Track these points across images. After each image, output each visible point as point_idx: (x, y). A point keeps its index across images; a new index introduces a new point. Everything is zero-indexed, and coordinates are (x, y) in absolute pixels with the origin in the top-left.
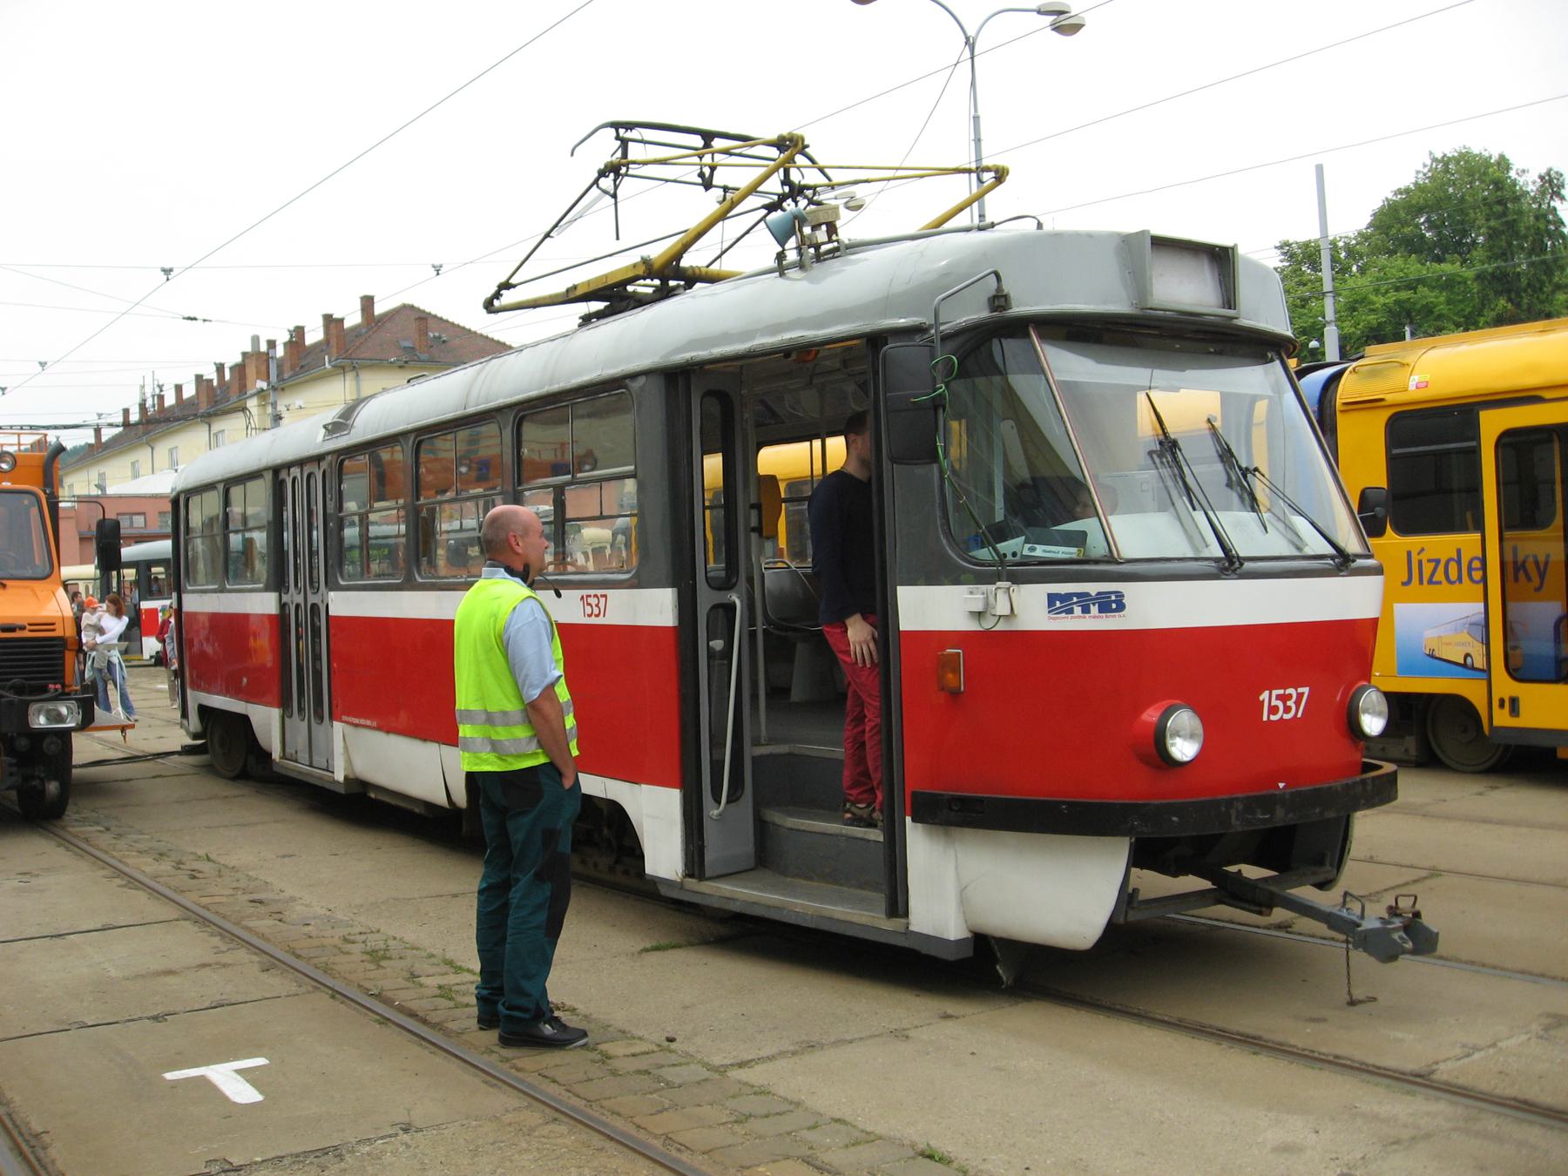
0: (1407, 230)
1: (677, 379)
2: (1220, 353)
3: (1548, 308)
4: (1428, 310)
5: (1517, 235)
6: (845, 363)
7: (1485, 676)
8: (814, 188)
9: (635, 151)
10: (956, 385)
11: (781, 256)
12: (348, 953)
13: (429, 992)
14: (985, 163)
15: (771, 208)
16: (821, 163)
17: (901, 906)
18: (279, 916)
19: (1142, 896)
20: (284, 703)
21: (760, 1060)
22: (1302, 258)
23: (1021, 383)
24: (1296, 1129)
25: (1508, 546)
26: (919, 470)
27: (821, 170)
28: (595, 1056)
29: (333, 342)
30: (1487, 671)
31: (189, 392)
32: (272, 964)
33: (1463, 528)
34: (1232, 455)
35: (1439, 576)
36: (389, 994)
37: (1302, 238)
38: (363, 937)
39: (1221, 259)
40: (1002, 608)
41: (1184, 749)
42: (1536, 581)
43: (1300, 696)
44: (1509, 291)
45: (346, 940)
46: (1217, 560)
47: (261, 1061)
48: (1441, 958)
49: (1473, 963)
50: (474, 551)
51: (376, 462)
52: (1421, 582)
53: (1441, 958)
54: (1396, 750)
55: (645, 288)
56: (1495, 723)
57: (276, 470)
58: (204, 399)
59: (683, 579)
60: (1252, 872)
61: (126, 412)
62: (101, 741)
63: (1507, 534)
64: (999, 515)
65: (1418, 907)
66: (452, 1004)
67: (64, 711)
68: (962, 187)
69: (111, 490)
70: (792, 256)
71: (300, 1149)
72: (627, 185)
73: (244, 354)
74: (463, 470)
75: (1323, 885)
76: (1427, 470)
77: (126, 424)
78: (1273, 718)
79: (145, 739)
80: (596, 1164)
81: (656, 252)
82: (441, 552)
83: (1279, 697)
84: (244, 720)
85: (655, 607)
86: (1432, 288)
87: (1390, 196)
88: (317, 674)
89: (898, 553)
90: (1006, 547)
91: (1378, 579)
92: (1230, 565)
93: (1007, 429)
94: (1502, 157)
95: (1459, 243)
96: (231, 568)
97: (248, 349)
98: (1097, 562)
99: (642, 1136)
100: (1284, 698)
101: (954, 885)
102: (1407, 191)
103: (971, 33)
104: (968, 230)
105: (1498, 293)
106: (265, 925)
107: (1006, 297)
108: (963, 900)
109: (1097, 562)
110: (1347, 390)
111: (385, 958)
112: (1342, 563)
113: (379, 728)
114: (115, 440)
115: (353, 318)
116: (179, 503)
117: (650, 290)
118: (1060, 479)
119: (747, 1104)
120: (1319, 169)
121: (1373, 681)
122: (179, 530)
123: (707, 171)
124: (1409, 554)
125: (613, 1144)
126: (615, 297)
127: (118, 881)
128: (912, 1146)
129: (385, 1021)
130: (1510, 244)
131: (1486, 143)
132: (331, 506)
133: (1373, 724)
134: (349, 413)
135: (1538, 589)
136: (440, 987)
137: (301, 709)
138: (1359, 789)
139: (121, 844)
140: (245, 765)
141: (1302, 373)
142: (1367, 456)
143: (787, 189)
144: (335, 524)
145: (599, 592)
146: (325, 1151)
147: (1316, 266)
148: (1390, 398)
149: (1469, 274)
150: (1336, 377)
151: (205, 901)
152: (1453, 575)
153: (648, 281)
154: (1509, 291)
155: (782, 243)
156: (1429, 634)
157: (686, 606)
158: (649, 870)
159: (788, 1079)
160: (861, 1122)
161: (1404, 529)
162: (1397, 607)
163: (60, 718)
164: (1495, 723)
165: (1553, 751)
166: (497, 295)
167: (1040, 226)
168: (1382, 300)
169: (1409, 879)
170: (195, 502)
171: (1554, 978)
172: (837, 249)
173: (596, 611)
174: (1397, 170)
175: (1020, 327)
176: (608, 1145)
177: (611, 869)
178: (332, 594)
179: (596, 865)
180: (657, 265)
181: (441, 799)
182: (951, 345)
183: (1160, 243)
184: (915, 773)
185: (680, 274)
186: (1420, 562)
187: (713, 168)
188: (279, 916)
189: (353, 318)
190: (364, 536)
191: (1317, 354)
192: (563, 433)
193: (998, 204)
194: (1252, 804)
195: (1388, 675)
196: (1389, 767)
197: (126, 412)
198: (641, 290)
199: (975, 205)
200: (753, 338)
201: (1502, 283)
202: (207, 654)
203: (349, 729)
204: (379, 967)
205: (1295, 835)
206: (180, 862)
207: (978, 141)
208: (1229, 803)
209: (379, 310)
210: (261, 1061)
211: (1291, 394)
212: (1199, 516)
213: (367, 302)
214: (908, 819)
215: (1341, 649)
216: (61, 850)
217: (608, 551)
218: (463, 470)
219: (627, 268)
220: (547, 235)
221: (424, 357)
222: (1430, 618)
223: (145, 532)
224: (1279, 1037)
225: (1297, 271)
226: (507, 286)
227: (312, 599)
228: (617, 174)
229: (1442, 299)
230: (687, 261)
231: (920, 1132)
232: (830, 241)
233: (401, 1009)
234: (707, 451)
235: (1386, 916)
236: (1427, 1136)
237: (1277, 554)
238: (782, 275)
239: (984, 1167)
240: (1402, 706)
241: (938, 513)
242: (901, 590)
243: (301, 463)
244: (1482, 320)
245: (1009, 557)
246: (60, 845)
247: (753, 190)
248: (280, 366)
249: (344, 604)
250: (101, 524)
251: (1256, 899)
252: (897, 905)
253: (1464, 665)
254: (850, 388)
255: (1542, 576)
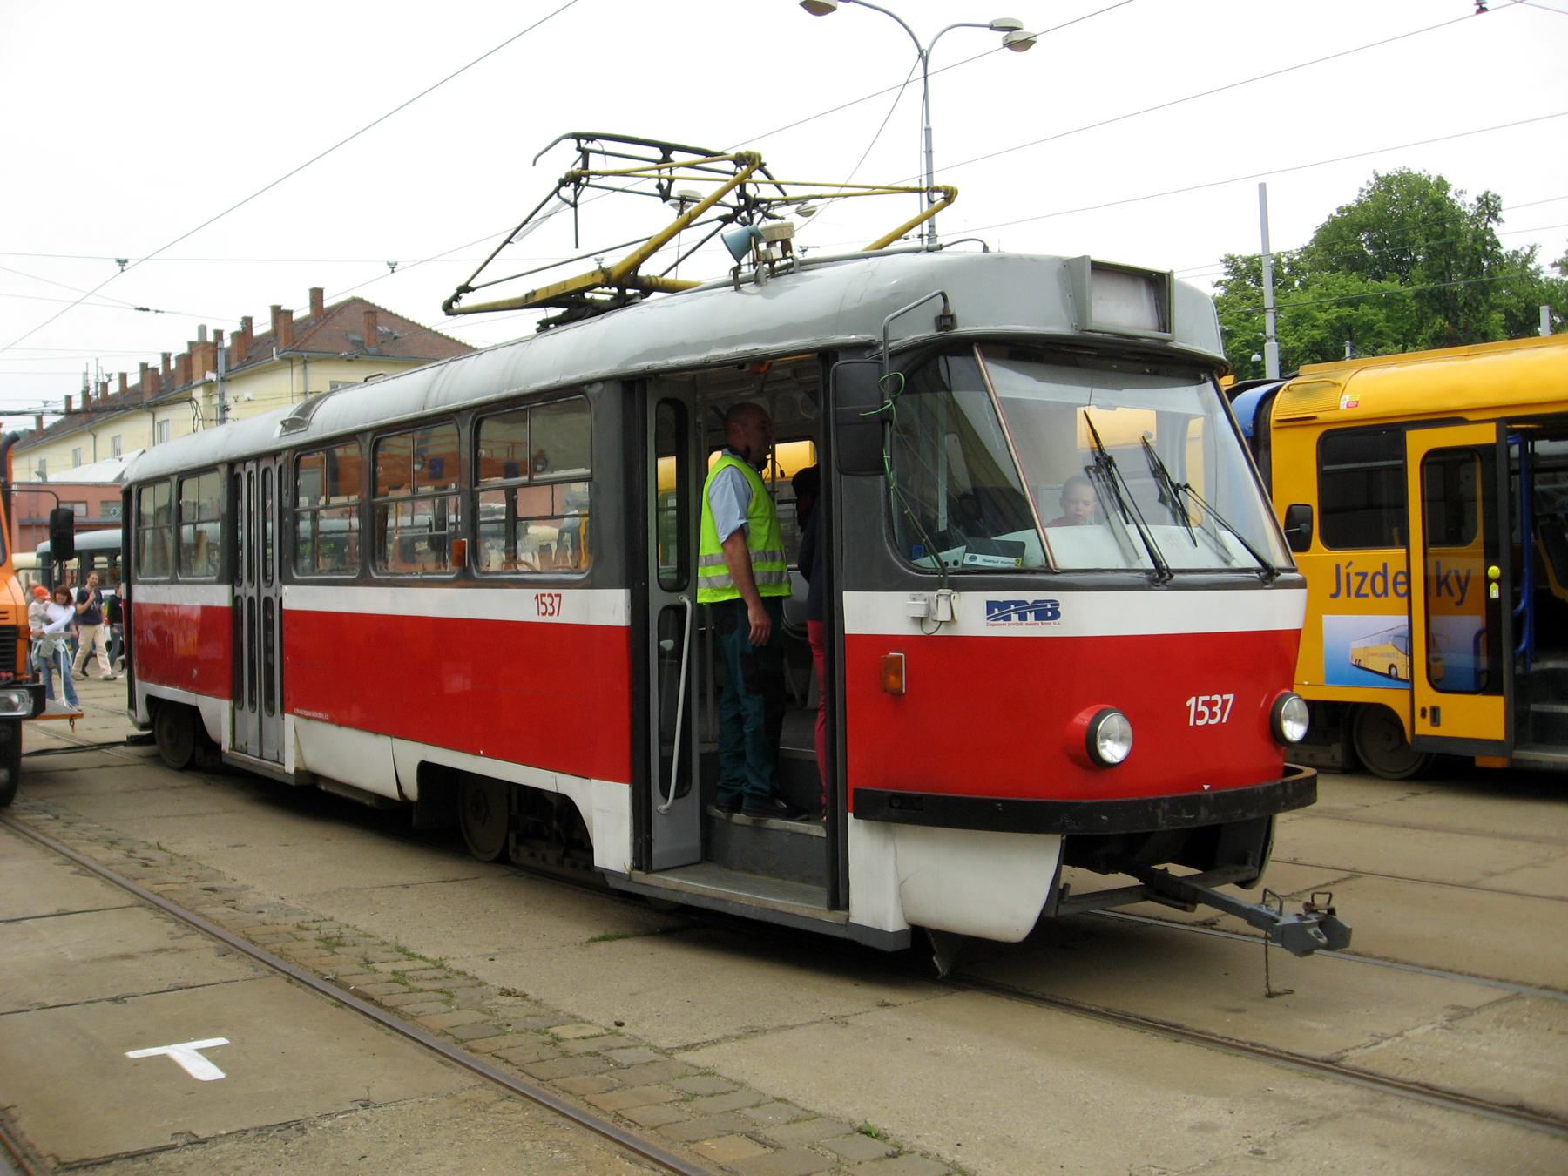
0: (1349, 247)
1: (633, 386)
2: (1155, 373)
3: (1483, 327)
4: (1368, 327)
5: (1455, 254)
6: (795, 373)
7: (1408, 686)
8: (769, 201)
9: (595, 163)
10: (902, 400)
11: (736, 270)
12: (302, 940)
13: (384, 978)
14: (937, 182)
15: (726, 220)
16: (778, 179)
17: (842, 902)
18: (233, 904)
19: (1072, 892)
20: (235, 696)
21: (706, 1043)
22: (1244, 272)
23: (966, 399)
24: (1211, 1109)
25: (1431, 561)
26: (866, 481)
27: (778, 186)
28: (547, 1038)
29: (281, 335)
30: (1410, 682)
31: (134, 380)
32: (228, 949)
33: (1389, 544)
34: (1165, 472)
35: (1366, 589)
36: (344, 979)
37: (1248, 253)
38: (315, 925)
39: (1157, 284)
40: (943, 614)
41: (1113, 751)
42: (1458, 596)
43: (1225, 702)
44: (1447, 309)
45: (299, 927)
46: (1148, 572)
47: (221, 1041)
48: (1356, 954)
49: (1385, 959)
50: (423, 546)
51: (332, 458)
52: (1349, 595)
53: (1356, 954)
54: (1323, 758)
55: (602, 295)
56: (1418, 731)
57: (232, 464)
58: (149, 388)
59: (635, 580)
60: (1178, 870)
61: (69, 399)
62: (45, 730)
63: (1431, 550)
64: (942, 525)
65: (1333, 904)
66: (406, 989)
67: (15, 699)
68: (912, 206)
69: (53, 478)
70: (747, 271)
71: (264, 1123)
72: (587, 193)
73: (191, 344)
74: (417, 467)
75: (1245, 884)
76: (1357, 486)
77: (69, 412)
78: (1199, 723)
79: (91, 730)
80: (549, 1137)
81: (613, 260)
82: (390, 547)
83: (1204, 703)
84: (194, 711)
85: (608, 607)
86: (1372, 305)
87: (1335, 213)
88: (270, 668)
89: (845, 560)
90: (948, 555)
91: (1302, 592)
92: (1160, 577)
93: (950, 442)
94: (1440, 178)
95: (1399, 261)
96: (179, 563)
97: (195, 338)
98: (1034, 572)
99: (592, 1112)
100: (1210, 704)
101: (895, 878)
102: (1349, 209)
103: (924, 46)
104: (917, 251)
105: (1437, 311)
106: (219, 911)
107: (952, 317)
108: (901, 895)
109: (1034, 572)
110: (1282, 407)
111: (338, 945)
112: (1267, 576)
113: (331, 721)
114: (56, 427)
115: (301, 309)
116: (130, 494)
117: (608, 297)
118: (1000, 490)
119: (694, 1084)
120: (1262, 187)
121: (1296, 688)
122: (130, 518)
123: (665, 183)
124: (1338, 567)
125: (565, 1120)
126: (573, 305)
127: (71, 868)
128: (851, 1123)
129: (341, 1004)
130: (1448, 264)
131: (1425, 164)
132: (287, 502)
133: (1294, 730)
134: (306, 410)
135: (1459, 603)
136: (394, 973)
137: (252, 702)
138: (1279, 792)
139: (71, 832)
140: (193, 755)
141: (1233, 393)
142: (1299, 476)
143: (742, 202)
144: (289, 517)
145: (554, 592)
146: (287, 1125)
147: (1258, 281)
148: (1322, 416)
149: (1408, 291)
150: (1271, 395)
151: (158, 888)
152: (1379, 588)
153: (606, 289)
154: (1447, 309)
155: (738, 259)
156: (1355, 645)
157: (639, 607)
158: (597, 863)
159: (732, 1061)
160: (802, 1101)
161: (1334, 540)
162: (1327, 619)
163: (11, 706)
164: (1418, 731)
165: (1472, 759)
166: (456, 298)
167: (986, 249)
168: (1325, 316)
169: (1331, 880)
170: (147, 493)
171: (1460, 973)
172: (791, 265)
173: (550, 610)
174: (1344, 189)
175: (966, 346)
176: (561, 1120)
177: (560, 862)
178: (286, 588)
179: (544, 859)
180: (615, 274)
181: (393, 792)
182: (898, 361)
183: (1100, 268)
184: (859, 770)
185: (637, 282)
186: (1348, 575)
187: (671, 181)
188: (233, 904)
189: (301, 309)
190: (315, 531)
191: (1258, 368)
192: (519, 433)
193: (948, 223)
194: (1176, 805)
195: (1312, 682)
196: (1309, 772)
197: (69, 399)
198: (598, 297)
199: (926, 223)
200: (709, 350)
201: (1440, 302)
202: (144, 646)
203: (301, 721)
204: (334, 953)
205: (1225, 838)
206: (131, 851)
207: (929, 152)
208: (1156, 803)
209: (327, 304)
210: (221, 1041)
211: (1222, 415)
212: (1132, 530)
213: (317, 294)
214: (850, 815)
215: (1264, 659)
216: (11, 838)
217: (554, 546)
218: (417, 467)
219: (585, 276)
221: (373, 350)
222: (1358, 629)
223: (86, 520)
224: (1199, 1026)
225: (1241, 286)
226: (466, 289)
227: (265, 592)
228: (578, 184)
229: (1381, 316)
230: (645, 271)
231: (856, 1111)
232: (785, 257)
233: (357, 993)
234: (661, 453)
235: (1302, 912)
236: (1334, 1117)
237: (1114, 567)
238: (737, 289)
239: (918, 1142)
240: (1320, 712)
241: (884, 522)
242: (848, 597)
243: (257, 458)
244: (1420, 338)
245: (951, 566)
246: (9, 833)
247: (716, 200)
248: (228, 358)
249: (297, 598)
250: (55, 514)
251: (1182, 895)
252: (839, 898)
253: (1389, 676)
254: (800, 396)
255: (1463, 591)
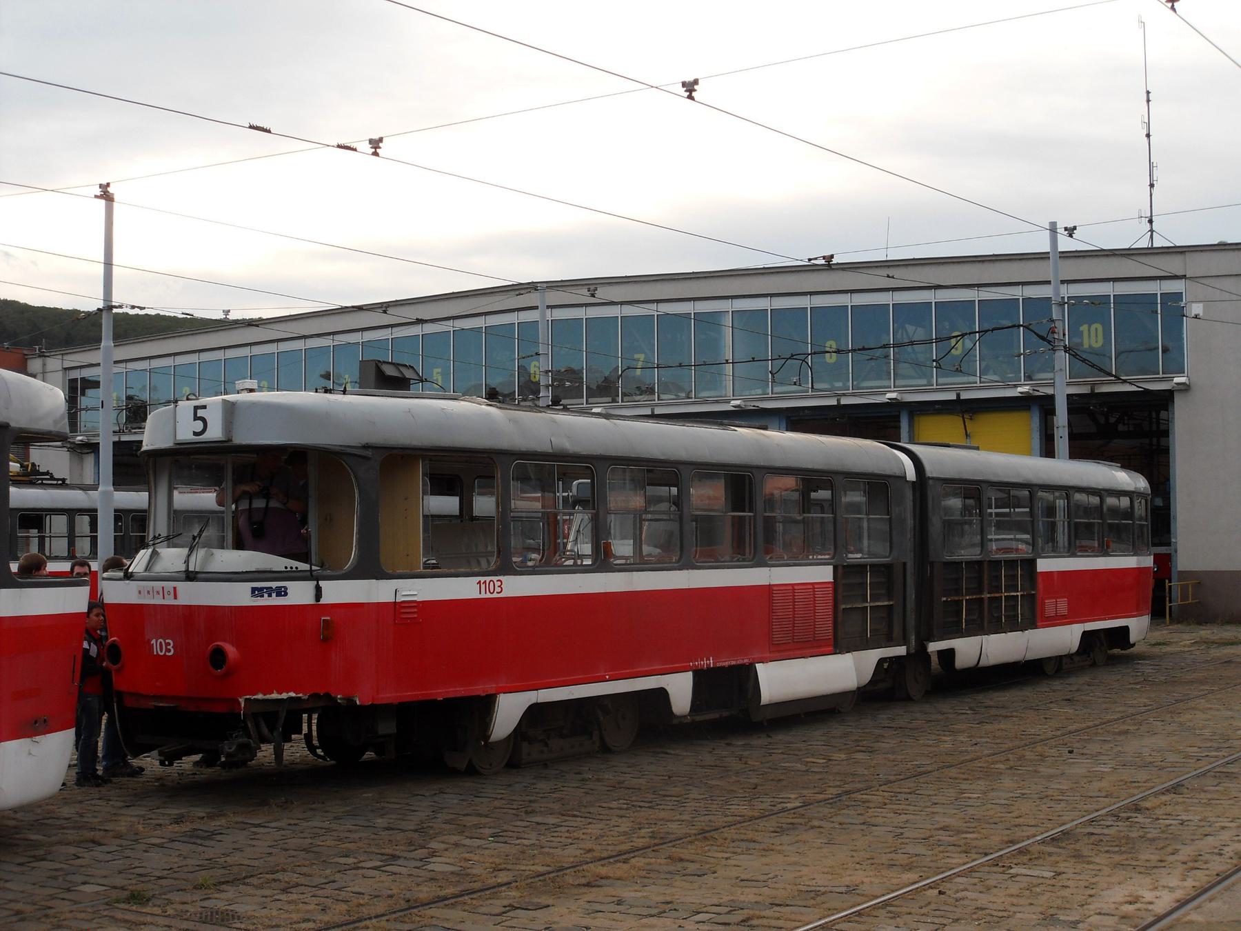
213: (227, 312)
220: (1148, 101)
